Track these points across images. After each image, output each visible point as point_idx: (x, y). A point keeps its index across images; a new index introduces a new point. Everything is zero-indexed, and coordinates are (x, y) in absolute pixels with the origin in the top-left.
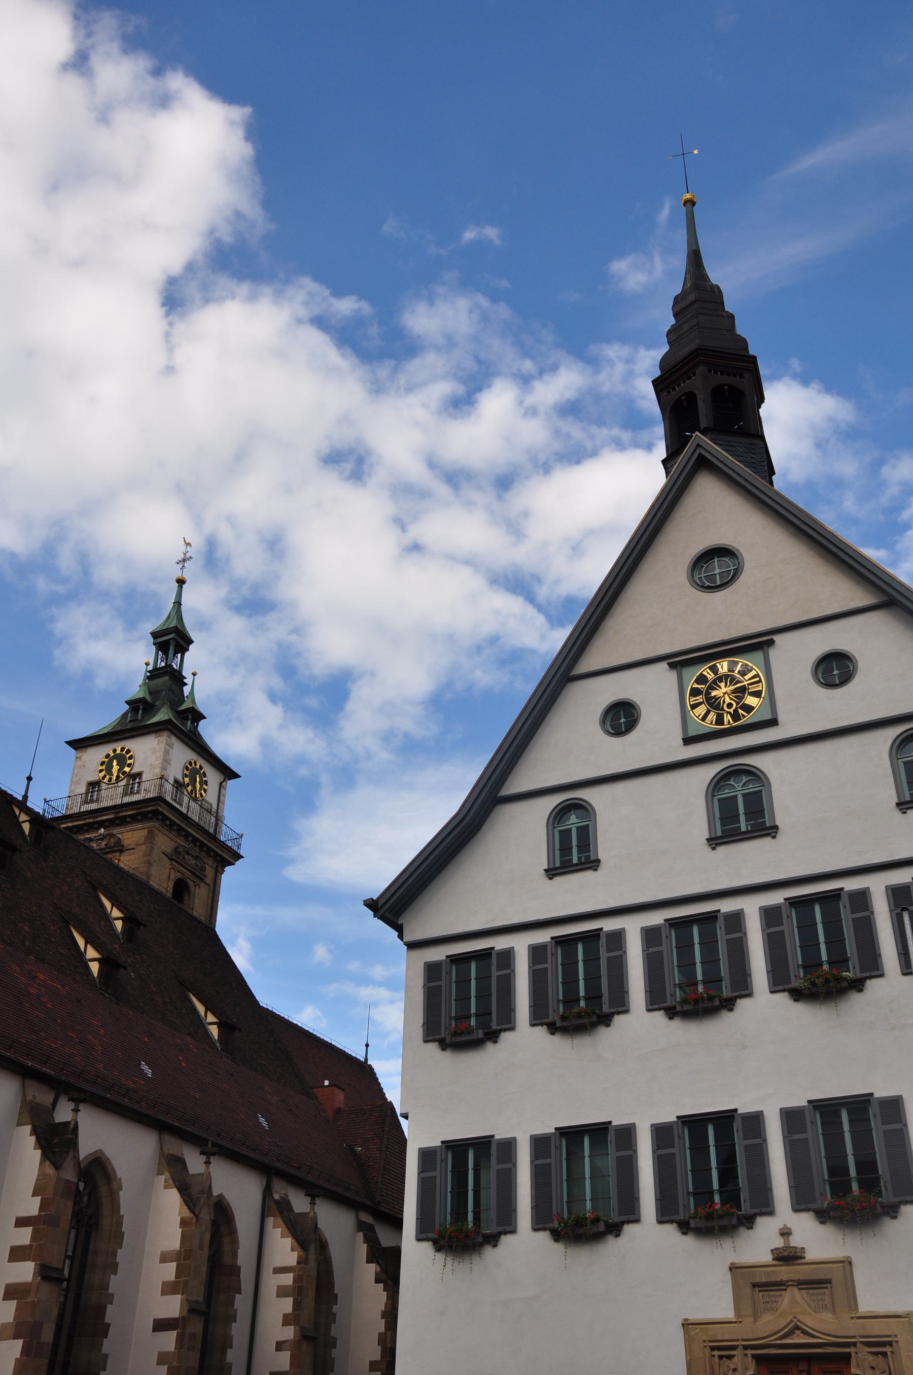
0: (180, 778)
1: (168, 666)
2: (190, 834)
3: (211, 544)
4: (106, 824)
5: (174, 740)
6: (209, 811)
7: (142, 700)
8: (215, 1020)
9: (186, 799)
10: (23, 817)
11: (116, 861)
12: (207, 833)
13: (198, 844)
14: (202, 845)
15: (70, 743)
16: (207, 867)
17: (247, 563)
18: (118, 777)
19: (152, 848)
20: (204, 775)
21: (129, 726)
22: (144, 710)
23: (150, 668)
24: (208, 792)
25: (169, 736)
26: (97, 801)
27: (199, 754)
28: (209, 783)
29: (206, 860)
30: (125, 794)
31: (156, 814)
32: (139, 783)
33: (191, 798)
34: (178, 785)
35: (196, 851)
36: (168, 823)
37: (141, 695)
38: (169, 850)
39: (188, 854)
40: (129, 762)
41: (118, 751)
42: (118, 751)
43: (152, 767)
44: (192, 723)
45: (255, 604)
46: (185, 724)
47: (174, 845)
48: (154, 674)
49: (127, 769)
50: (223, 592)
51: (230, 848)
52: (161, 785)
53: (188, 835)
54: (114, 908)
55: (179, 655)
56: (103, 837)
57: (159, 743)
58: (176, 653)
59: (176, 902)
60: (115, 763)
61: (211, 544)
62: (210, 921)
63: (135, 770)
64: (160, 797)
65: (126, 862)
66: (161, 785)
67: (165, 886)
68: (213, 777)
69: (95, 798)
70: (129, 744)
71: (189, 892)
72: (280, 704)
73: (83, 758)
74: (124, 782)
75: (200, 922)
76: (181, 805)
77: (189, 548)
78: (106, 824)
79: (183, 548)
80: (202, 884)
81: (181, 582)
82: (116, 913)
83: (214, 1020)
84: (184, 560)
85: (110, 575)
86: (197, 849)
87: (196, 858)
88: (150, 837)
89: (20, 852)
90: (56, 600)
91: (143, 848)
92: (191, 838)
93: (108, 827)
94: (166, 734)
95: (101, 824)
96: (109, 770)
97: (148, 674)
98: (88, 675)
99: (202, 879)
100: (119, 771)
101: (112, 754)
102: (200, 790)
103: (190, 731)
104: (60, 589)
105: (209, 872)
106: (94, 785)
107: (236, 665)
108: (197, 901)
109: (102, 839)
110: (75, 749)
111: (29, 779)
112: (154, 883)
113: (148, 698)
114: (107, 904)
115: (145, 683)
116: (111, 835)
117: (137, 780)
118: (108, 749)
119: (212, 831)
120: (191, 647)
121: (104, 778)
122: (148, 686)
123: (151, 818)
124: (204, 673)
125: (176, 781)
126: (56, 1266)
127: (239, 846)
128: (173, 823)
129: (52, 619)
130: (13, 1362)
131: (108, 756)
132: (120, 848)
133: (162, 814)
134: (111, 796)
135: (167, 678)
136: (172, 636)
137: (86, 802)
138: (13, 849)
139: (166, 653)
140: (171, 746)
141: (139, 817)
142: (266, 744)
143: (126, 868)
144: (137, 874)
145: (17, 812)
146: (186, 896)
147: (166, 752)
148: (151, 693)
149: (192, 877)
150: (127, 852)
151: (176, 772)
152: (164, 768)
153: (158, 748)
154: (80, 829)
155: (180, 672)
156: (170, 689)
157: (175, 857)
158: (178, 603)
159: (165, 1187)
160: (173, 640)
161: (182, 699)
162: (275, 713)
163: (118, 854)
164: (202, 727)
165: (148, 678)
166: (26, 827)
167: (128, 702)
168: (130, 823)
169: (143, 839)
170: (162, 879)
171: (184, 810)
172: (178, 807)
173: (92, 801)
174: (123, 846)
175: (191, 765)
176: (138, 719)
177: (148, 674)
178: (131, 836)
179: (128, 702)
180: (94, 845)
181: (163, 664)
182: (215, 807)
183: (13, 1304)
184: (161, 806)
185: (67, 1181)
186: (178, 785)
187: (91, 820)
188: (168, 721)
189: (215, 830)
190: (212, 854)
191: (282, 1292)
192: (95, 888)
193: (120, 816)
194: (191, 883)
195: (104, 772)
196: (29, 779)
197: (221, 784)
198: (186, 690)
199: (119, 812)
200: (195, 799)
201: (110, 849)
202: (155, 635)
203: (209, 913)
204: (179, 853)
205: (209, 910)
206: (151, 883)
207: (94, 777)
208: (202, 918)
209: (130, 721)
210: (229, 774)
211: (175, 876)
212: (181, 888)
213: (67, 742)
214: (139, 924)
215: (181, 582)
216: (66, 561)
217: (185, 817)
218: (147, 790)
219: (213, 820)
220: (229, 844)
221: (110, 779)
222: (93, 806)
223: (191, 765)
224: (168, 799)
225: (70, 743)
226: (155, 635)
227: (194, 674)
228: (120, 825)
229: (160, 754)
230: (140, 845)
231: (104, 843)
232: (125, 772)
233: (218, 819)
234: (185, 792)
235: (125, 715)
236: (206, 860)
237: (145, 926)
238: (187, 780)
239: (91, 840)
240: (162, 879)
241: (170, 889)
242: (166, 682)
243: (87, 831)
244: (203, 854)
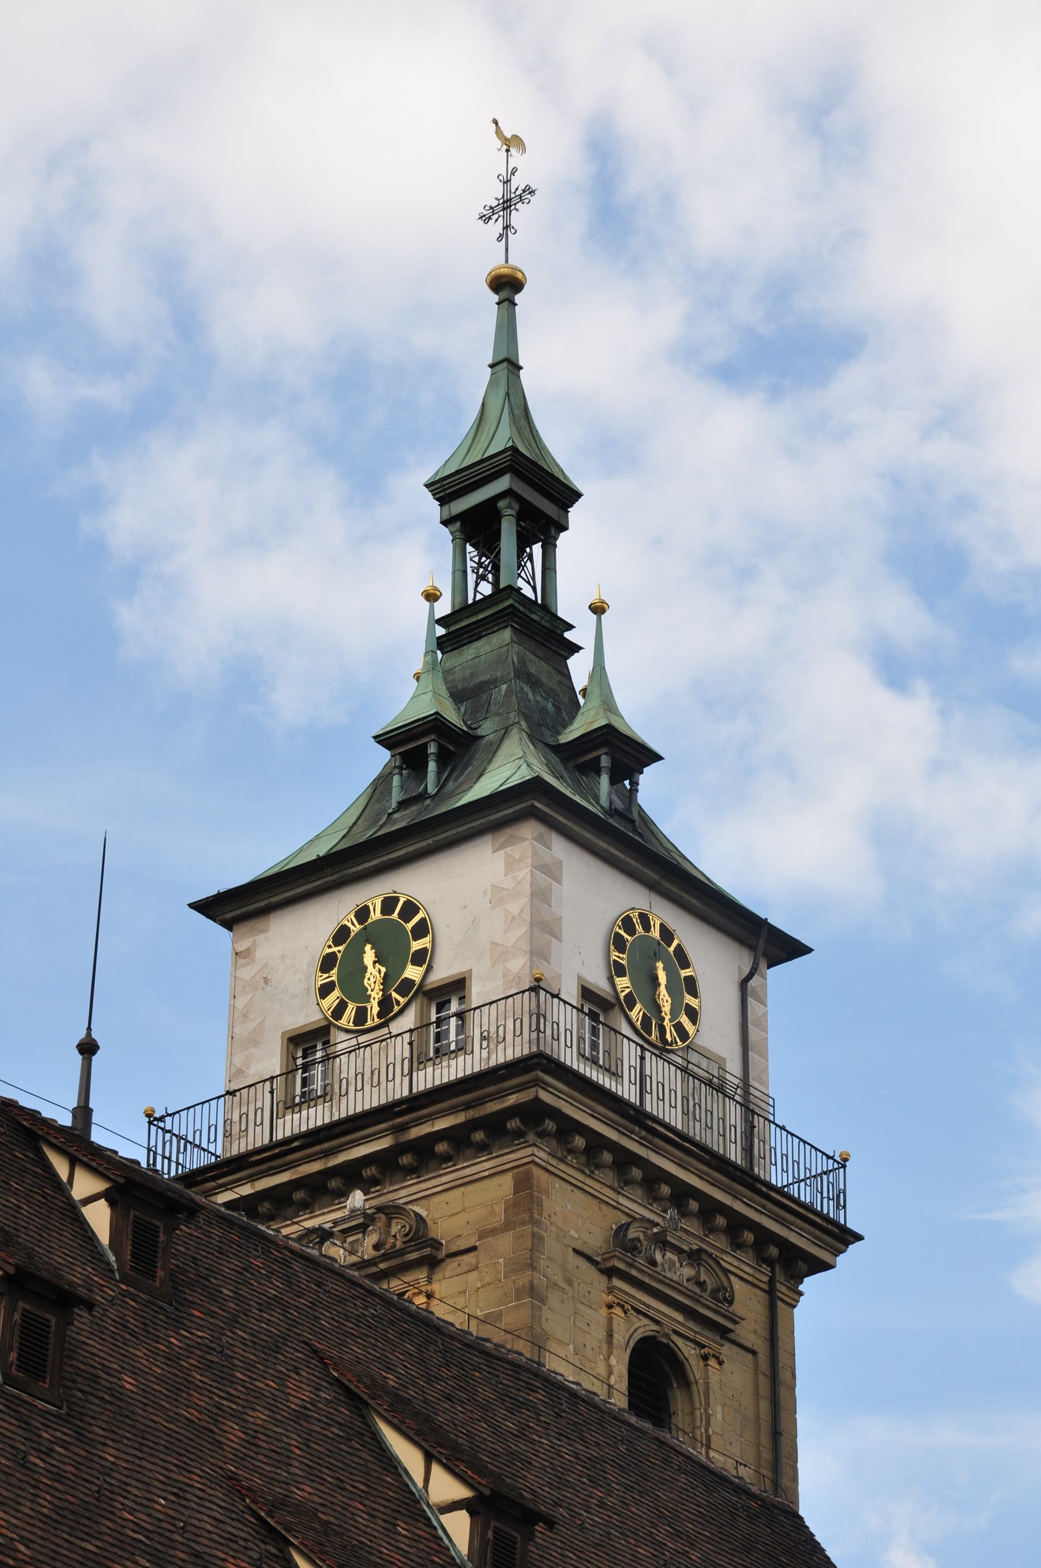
0: (599, 981)
1: (505, 592)
2: (660, 1176)
3: (604, 153)
4: (368, 1172)
5: (560, 849)
6: (719, 1088)
7: (434, 725)
8: (462, 1492)
9: (629, 1053)
10: (84, 1185)
11: (420, 1300)
12: (719, 1163)
13: (694, 1205)
14: (709, 1209)
15: (208, 907)
16: (737, 1285)
17: (738, 199)
18: (386, 1003)
19: (537, 1240)
20: (682, 959)
21: (401, 820)
22: (444, 759)
23: (444, 607)
24: (704, 1018)
25: (540, 839)
26: (326, 1096)
27: (652, 887)
28: (702, 986)
29: (729, 1261)
30: (418, 1060)
31: (535, 1114)
32: (460, 1015)
33: (646, 1045)
34: (596, 1005)
35: (689, 1232)
36: (579, 1142)
37: (425, 709)
38: (596, 1240)
39: (664, 1244)
40: (416, 945)
41: (376, 915)
42: (376, 915)
43: (500, 953)
44: (615, 780)
45: (785, 346)
46: (596, 787)
47: (613, 1219)
48: (458, 630)
49: (413, 972)
50: (669, 319)
51: (809, 1208)
52: (539, 1015)
53: (653, 1177)
54: (436, 1470)
55: (537, 549)
56: (364, 1223)
57: (510, 867)
58: (524, 543)
59: (647, 1425)
60: (369, 956)
61: (604, 153)
62: (776, 1485)
63: (443, 972)
64: (540, 1055)
65: (454, 1298)
66: (539, 1015)
67: (601, 1369)
68: (713, 961)
69: (318, 1086)
70: (413, 883)
71: (686, 1383)
72: (921, 686)
73: (260, 954)
74: (408, 1021)
75: (741, 1490)
76: (616, 1075)
77: (516, 158)
78: (368, 1172)
79: (496, 161)
80: (727, 1350)
81: (506, 285)
82: (444, 1487)
83: (462, 1492)
84: (507, 205)
85: (267, 320)
86: (693, 1226)
87: (695, 1257)
88: (525, 1198)
89: (90, 1306)
90: (101, 433)
91: (505, 1243)
92: (665, 1190)
93: (375, 1182)
94: (529, 830)
95: (352, 1176)
96: (353, 973)
97: (440, 631)
98: (245, 679)
99: (724, 1333)
100: (386, 981)
101: (355, 928)
102: (674, 1013)
103: (613, 812)
104: (110, 393)
105: (748, 1303)
106: (308, 1043)
107: (746, 574)
108: (718, 1413)
109: (363, 1228)
110: (228, 925)
111: (88, 1048)
112: (559, 1364)
113: (452, 716)
114: (408, 1455)
115: (432, 666)
116: (391, 1211)
117: (454, 1007)
119: (735, 1154)
120: (575, 513)
121: (339, 1011)
122: (447, 673)
123: (519, 1134)
124: (631, 606)
125: (587, 993)
127: (840, 1199)
128: (596, 1144)
129: (96, 500)
131: (341, 935)
132: (426, 1252)
133: (555, 1114)
134: (372, 1074)
135: (507, 634)
136: (503, 484)
137: (291, 1106)
138: (65, 1300)
139: (489, 545)
140: (552, 871)
141: (479, 1136)
142: (890, 836)
143: (458, 1321)
144: (498, 1337)
145: (61, 1167)
146: (678, 1401)
147: (540, 895)
148: (458, 696)
149: (691, 1328)
150: (451, 1266)
151: (582, 961)
152: (539, 953)
153: (508, 884)
154: (282, 1202)
155: (546, 608)
156: (522, 674)
157: (620, 1261)
158: (507, 365)
160: (508, 499)
161: (568, 704)
162: (909, 722)
163: (421, 1274)
164: (652, 789)
165: (442, 643)
166: (99, 1218)
167: (385, 740)
168: (447, 1158)
169: (500, 1209)
170: (588, 1350)
171: (628, 1092)
172: (606, 1081)
173: (308, 1099)
174: (436, 1244)
175: (631, 931)
176: (427, 790)
177: (440, 631)
178: (458, 1202)
179: (385, 740)
180: (336, 1252)
181: (486, 589)
182: (734, 1067)
184: (546, 1086)
186: (596, 1005)
187: (316, 1167)
188: (534, 787)
189: (748, 1150)
190: (749, 1237)
192: (358, 1405)
193: (417, 1137)
194: (688, 1351)
195: (336, 993)
196: (88, 1048)
197: (744, 984)
198: (579, 668)
199: (404, 1128)
200: (663, 1050)
201: (394, 1262)
202: (444, 489)
203: (766, 1455)
204: (632, 1247)
205: (765, 1440)
206: (553, 1364)
207: (308, 1014)
208: (743, 1472)
209: (403, 805)
210: (769, 944)
211: (629, 1330)
212: (655, 1372)
213: (192, 906)
214: (528, 1517)
215: (506, 285)
216: (112, 293)
217: (634, 1116)
218: (491, 1042)
219: (734, 1114)
220: (805, 1194)
221: (361, 1016)
222: (317, 1116)
223: (631, 931)
224: (569, 1058)
225: (208, 907)
226: (444, 489)
227: (598, 609)
229: (520, 905)
230: (493, 1232)
231: (372, 1239)
232: (409, 983)
233: (753, 1112)
234: (626, 1029)
235: (381, 784)
236: (729, 1261)
237: (550, 1524)
238: (623, 983)
239: (323, 1235)
240: (588, 1350)
241: (620, 1379)
242: (507, 637)
243: (306, 1206)
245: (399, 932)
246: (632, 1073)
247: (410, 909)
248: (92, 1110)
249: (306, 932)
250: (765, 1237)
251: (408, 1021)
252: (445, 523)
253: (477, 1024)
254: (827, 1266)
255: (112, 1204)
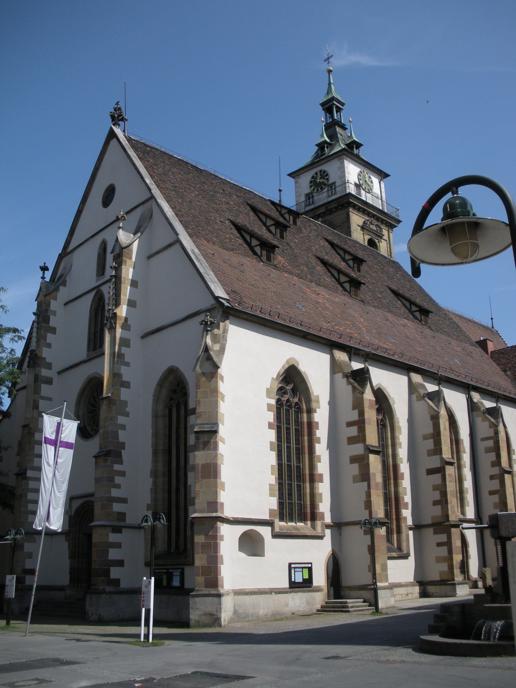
0: (357, 182)
2: (370, 213)
4: (322, 215)
15: (290, 175)
22: (327, 147)
26: (313, 203)
38: (361, 224)
47: (363, 220)
63: (331, 182)
70: (324, 167)
84: (328, 58)
110: (293, 178)
118: (312, 173)
119: (381, 208)
121: (314, 190)
126: (375, 445)
130: (363, 503)
131: (313, 177)
141: (340, 207)
159: (418, 401)
167: (317, 145)
173: (310, 205)
179: (317, 145)
181: (331, 120)
183: (356, 466)
185: (370, 400)
191: (488, 450)
194: (377, 241)
195: (313, 187)
202: (323, 105)
212: (372, 243)
217: (365, 203)
219: (380, 201)
224: (353, 193)
225: (290, 175)
228: (330, 214)
244: (379, 224)
245: (324, 174)
246: (364, 196)
247: (324, 172)
248: (400, 427)
249: (306, 178)
250: (387, 222)
251: (326, 190)
252: (323, 110)
253: (337, 189)
254: (397, 226)
255: (261, 247)
